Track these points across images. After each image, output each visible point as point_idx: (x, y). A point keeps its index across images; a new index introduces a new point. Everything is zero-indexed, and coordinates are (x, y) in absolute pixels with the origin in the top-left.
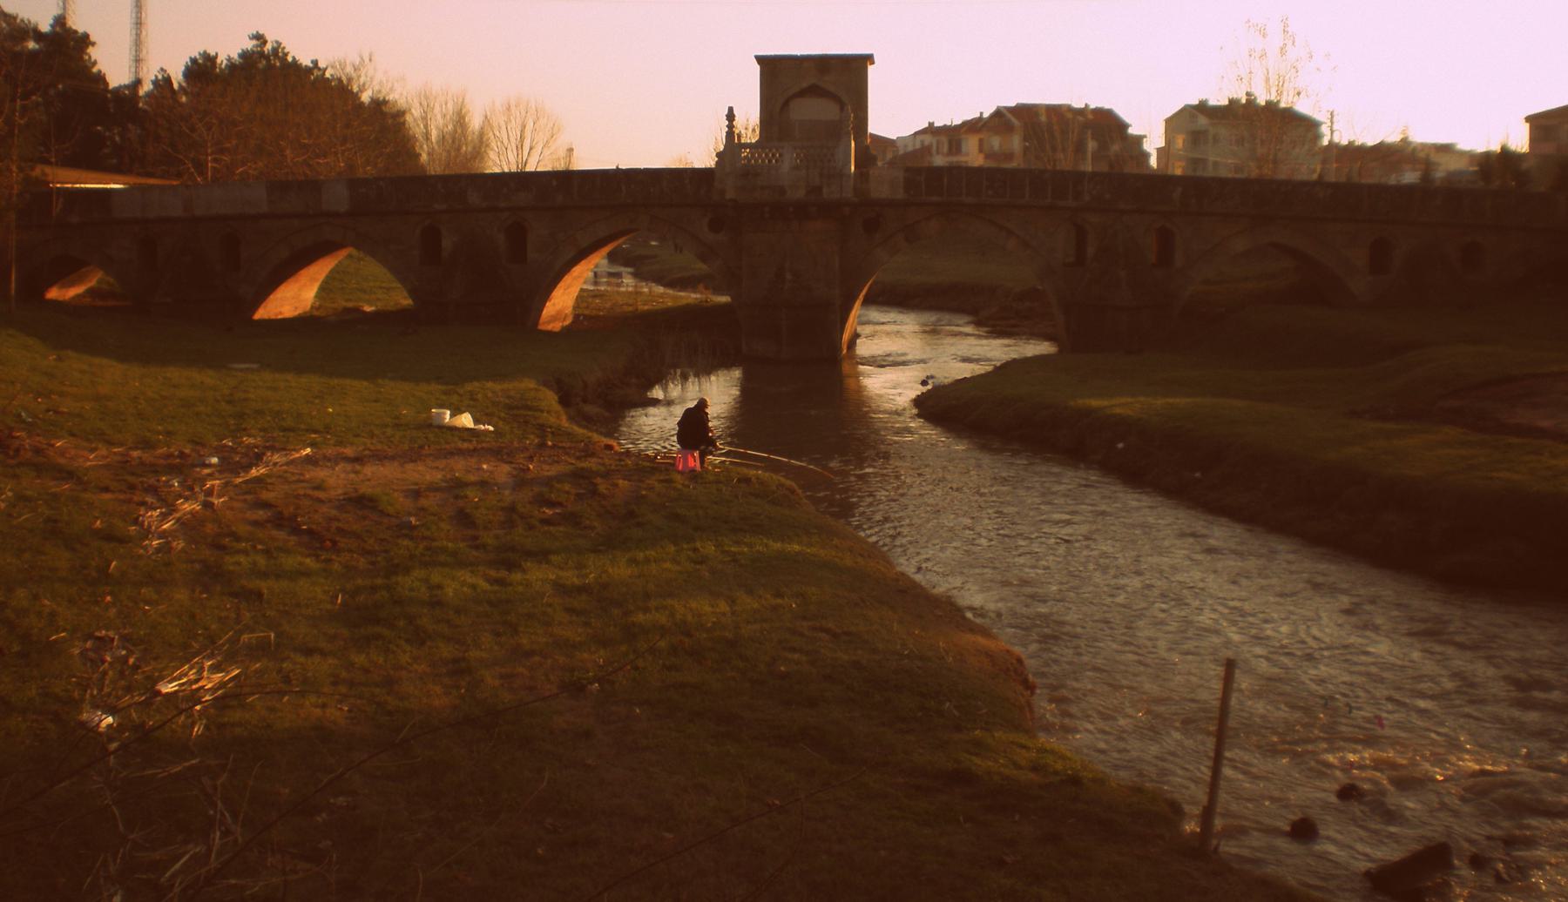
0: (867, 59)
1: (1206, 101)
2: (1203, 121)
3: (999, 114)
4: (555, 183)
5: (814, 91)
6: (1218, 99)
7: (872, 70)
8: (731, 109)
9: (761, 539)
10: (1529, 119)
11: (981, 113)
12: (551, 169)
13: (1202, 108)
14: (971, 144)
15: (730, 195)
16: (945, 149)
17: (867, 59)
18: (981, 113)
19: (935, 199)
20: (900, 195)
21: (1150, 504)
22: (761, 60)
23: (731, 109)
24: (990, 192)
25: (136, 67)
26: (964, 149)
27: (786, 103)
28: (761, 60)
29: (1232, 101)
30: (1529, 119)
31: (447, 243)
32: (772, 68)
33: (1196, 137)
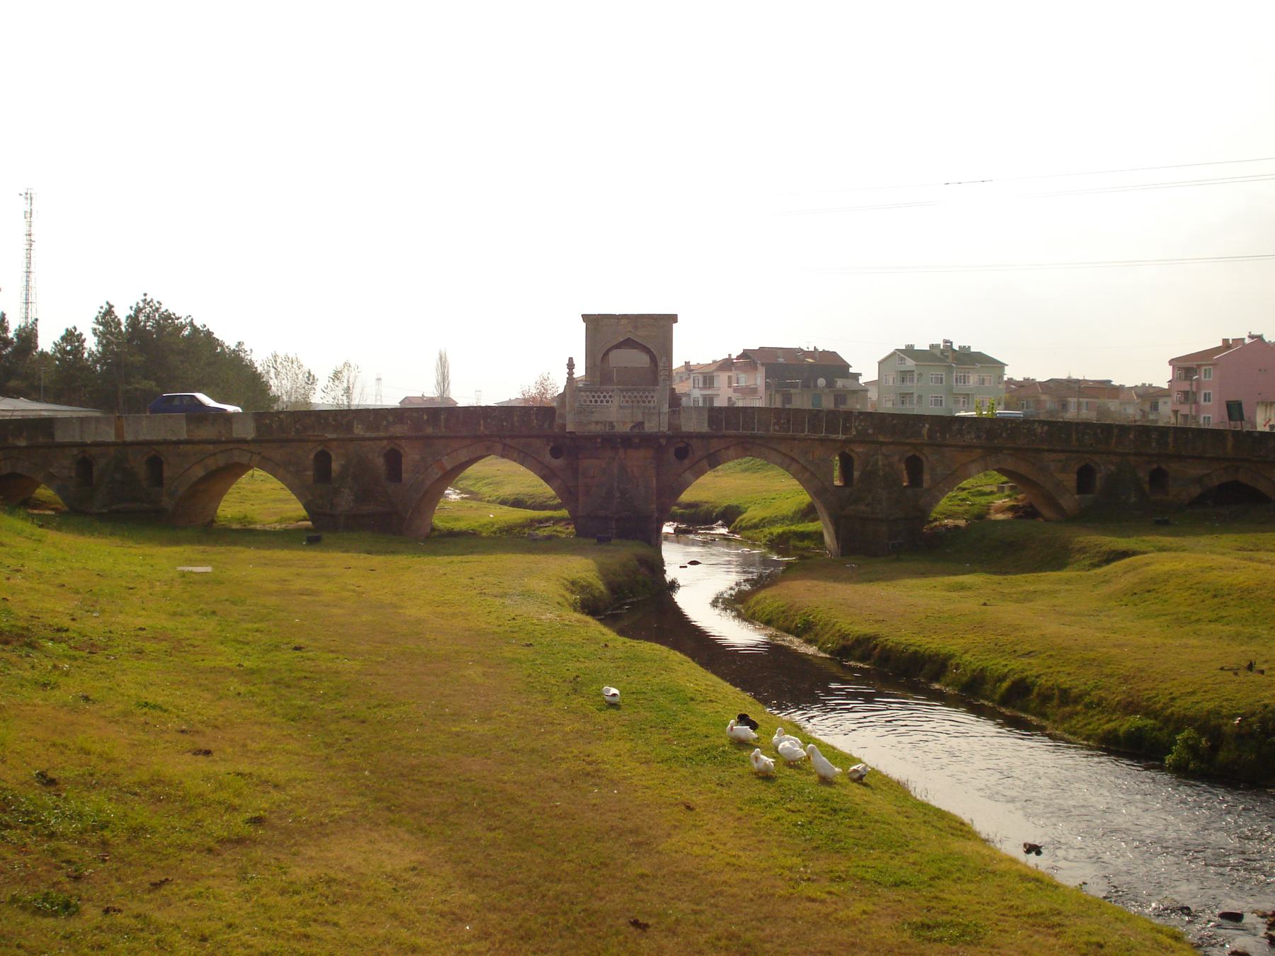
0: (673, 318)
1: (912, 346)
2: (910, 363)
3: (746, 354)
4: (425, 417)
5: (628, 343)
6: (922, 345)
7: (676, 327)
8: (571, 360)
9: (833, 643)
10: (1171, 362)
11: (730, 355)
12: (692, 430)
13: (910, 351)
14: (722, 379)
15: (570, 428)
16: (701, 385)
17: (673, 318)
18: (730, 355)
19: (732, 432)
20: (705, 428)
21: (1149, 568)
22: (586, 318)
23: (571, 360)
24: (777, 427)
25: (27, 309)
26: (716, 385)
27: (606, 353)
28: (586, 318)
29: (932, 346)
30: (1171, 362)
31: (335, 466)
32: (594, 323)
33: (904, 375)
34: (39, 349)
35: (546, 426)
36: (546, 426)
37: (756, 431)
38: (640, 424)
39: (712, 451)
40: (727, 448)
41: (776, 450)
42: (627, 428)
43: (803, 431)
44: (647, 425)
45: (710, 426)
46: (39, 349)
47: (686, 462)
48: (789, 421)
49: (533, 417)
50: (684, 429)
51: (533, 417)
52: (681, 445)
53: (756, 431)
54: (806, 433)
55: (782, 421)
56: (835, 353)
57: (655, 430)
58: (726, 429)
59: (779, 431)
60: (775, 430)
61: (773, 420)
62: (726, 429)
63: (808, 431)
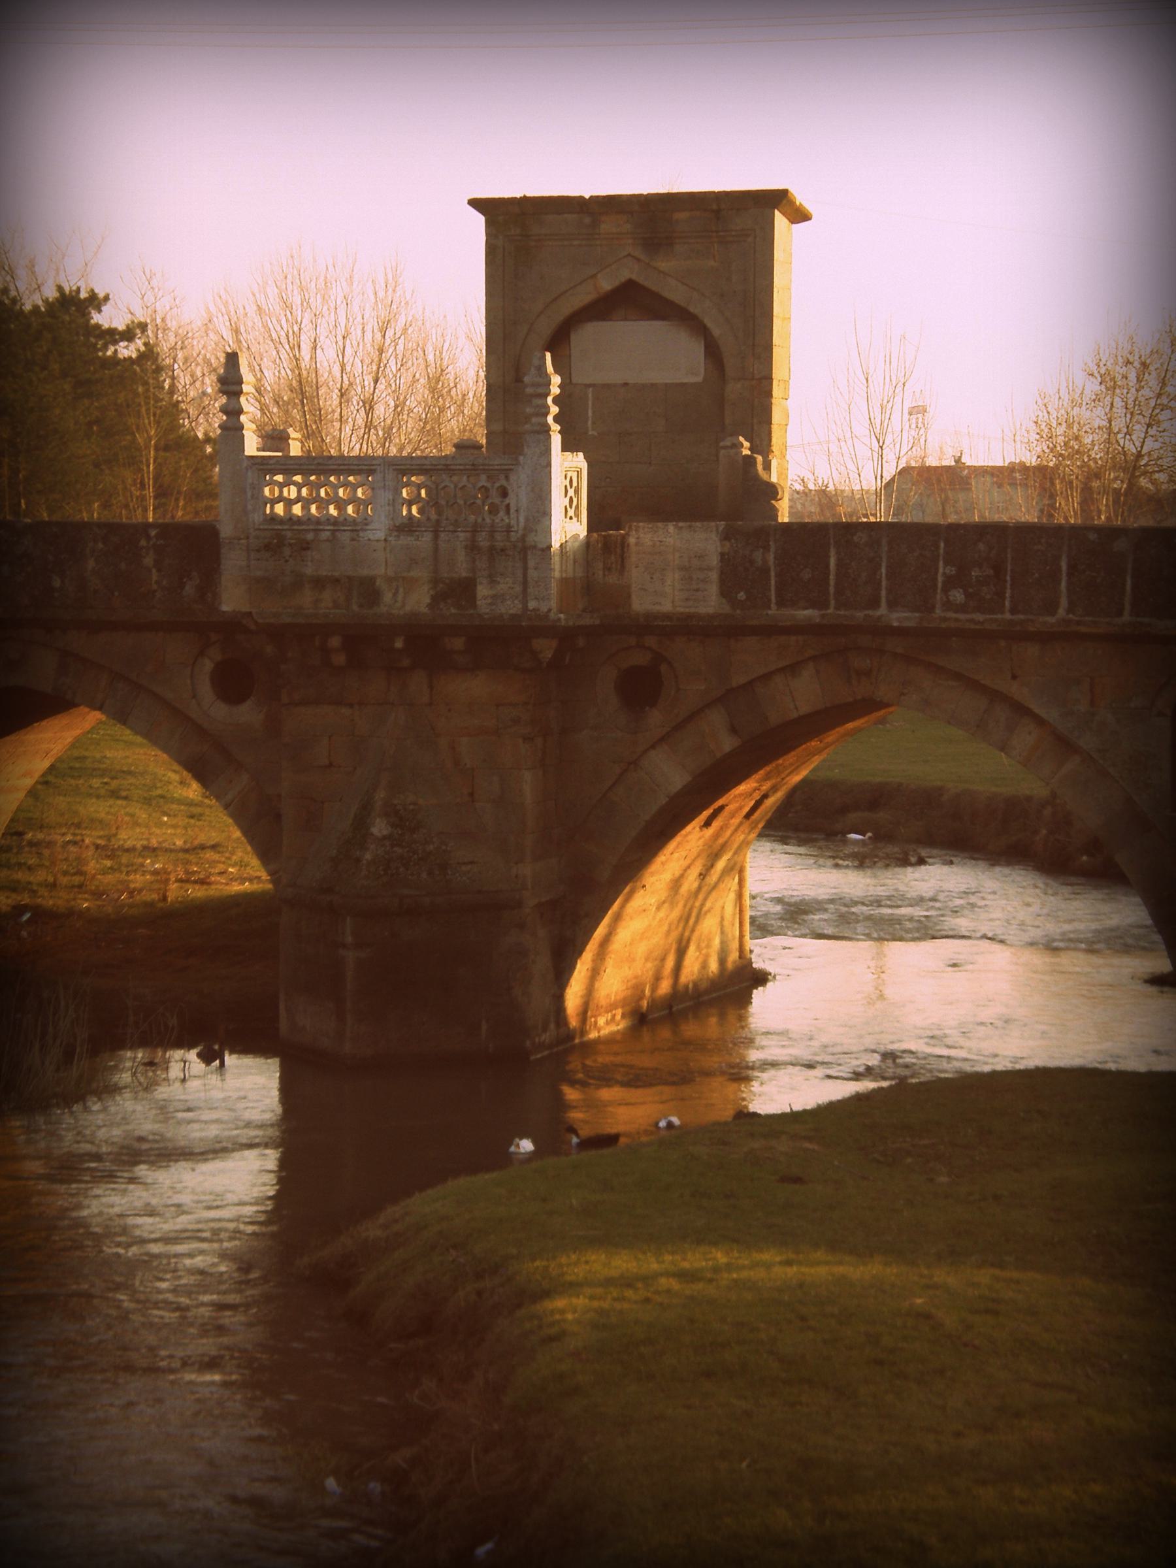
20: (711, 603)
24: (958, 596)
34: (746, 1052)
35: (189, 590)
36: (189, 590)
37: (883, 610)
38: (463, 590)
39: (738, 680)
40: (792, 669)
41: (958, 676)
42: (418, 601)
43: (1050, 607)
44: (483, 591)
45: (726, 591)
46: (746, 1052)
47: (656, 719)
48: (998, 569)
49: (149, 561)
50: (640, 604)
51: (149, 561)
52: (640, 659)
53: (773, 611)
54: (1061, 612)
55: (975, 573)
56: (525, 196)
57: (511, 607)
58: (781, 603)
59: (962, 609)
60: (948, 605)
61: (943, 570)
62: (781, 603)
63: (1070, 610)
